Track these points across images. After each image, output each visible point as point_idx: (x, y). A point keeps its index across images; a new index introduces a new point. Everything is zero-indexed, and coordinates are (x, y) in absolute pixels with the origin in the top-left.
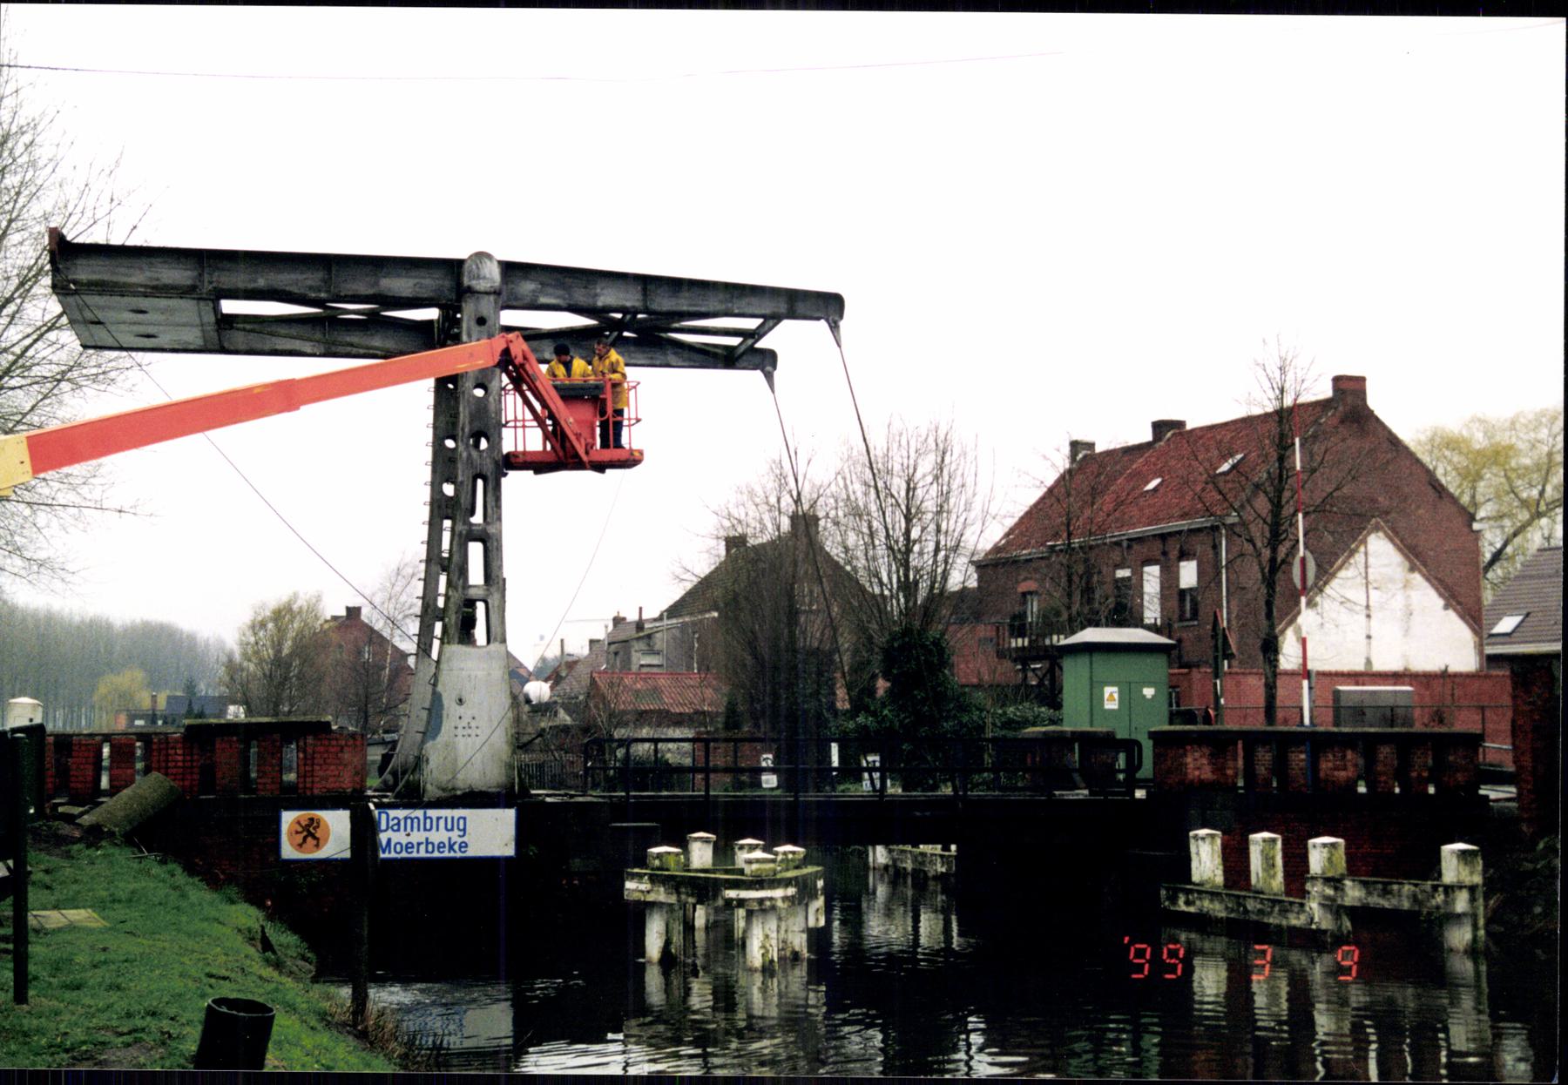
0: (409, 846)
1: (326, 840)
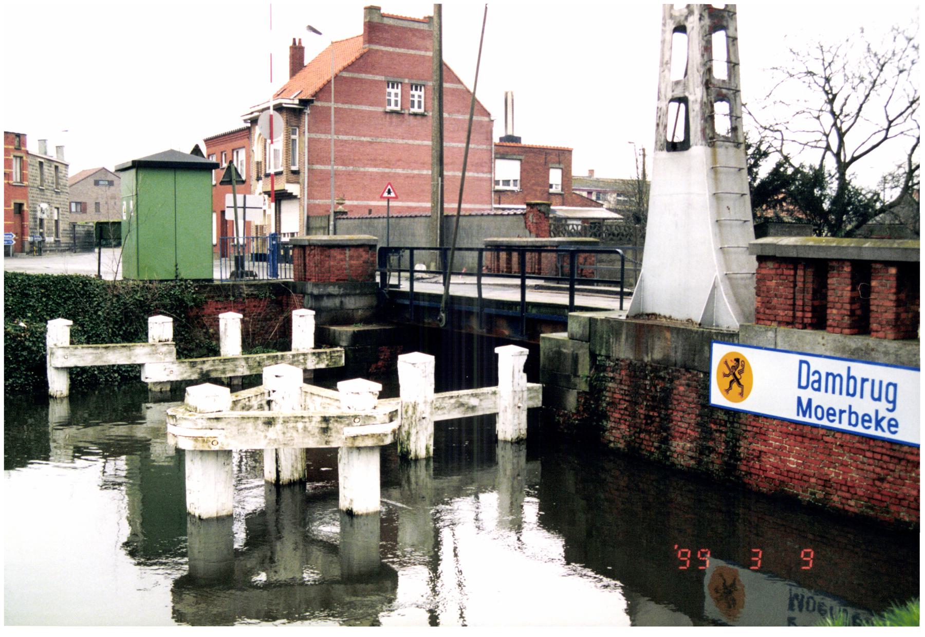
0: (830, 412)
1: (720, 363)
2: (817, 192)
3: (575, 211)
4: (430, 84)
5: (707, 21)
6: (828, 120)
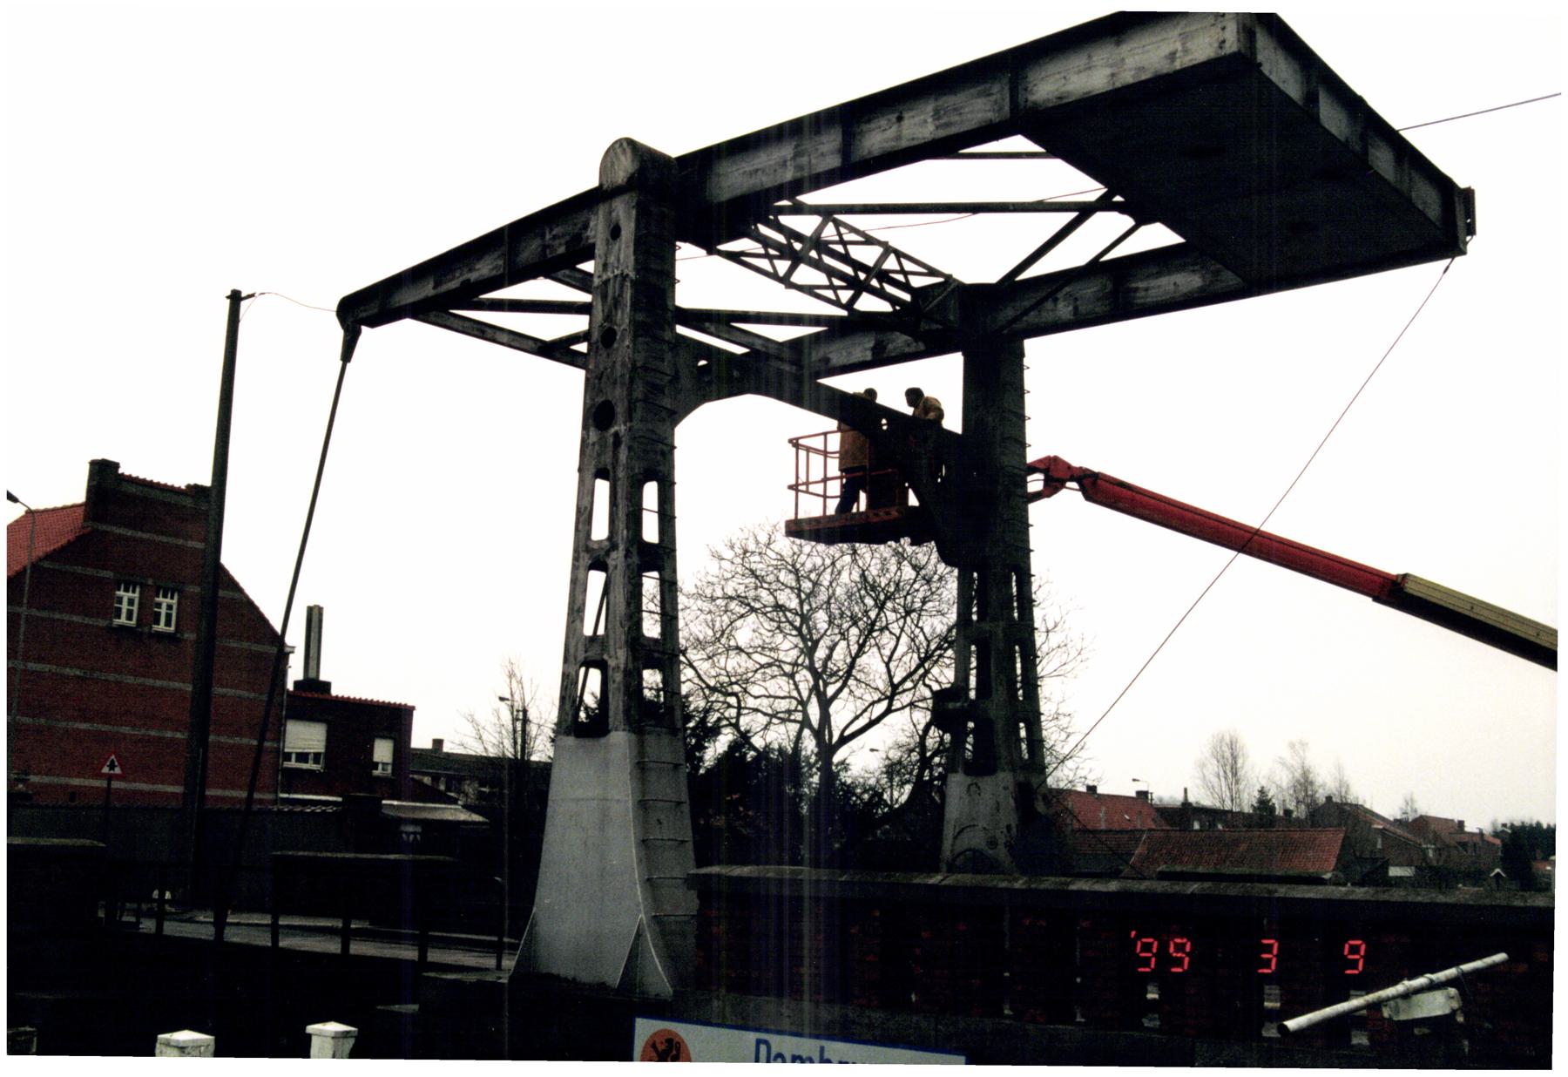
2: (789, 790)
3: (414, 808)
4: (193, 589)
5: (635, 559)
6: (805, 678)
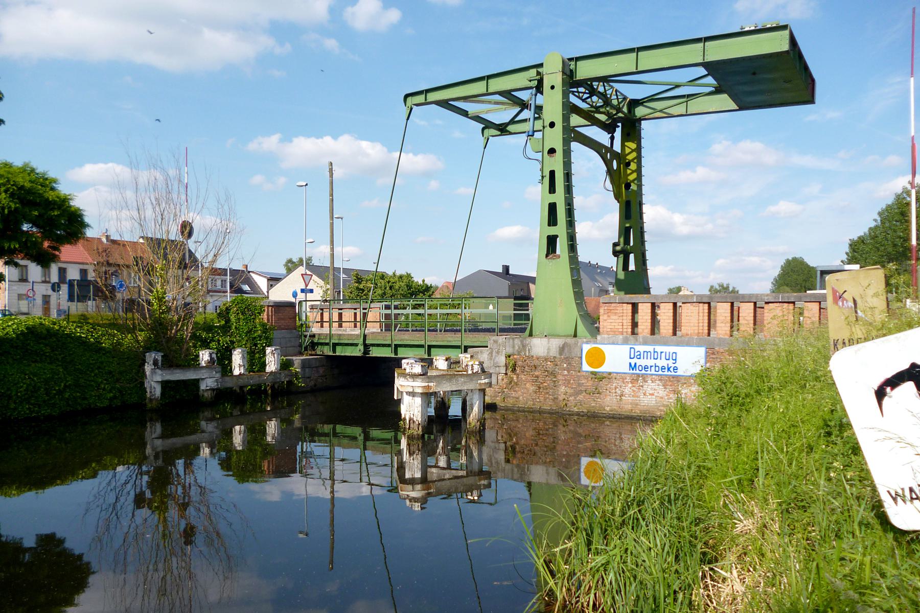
0: (646, 367)
